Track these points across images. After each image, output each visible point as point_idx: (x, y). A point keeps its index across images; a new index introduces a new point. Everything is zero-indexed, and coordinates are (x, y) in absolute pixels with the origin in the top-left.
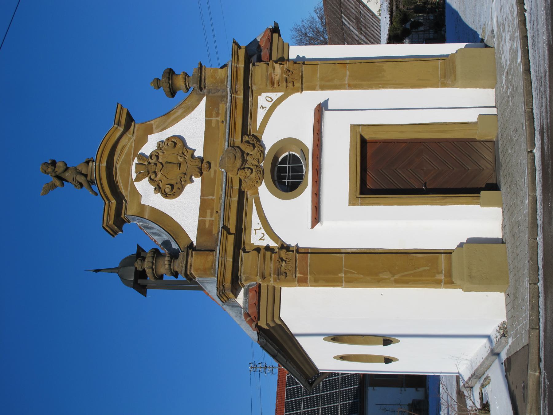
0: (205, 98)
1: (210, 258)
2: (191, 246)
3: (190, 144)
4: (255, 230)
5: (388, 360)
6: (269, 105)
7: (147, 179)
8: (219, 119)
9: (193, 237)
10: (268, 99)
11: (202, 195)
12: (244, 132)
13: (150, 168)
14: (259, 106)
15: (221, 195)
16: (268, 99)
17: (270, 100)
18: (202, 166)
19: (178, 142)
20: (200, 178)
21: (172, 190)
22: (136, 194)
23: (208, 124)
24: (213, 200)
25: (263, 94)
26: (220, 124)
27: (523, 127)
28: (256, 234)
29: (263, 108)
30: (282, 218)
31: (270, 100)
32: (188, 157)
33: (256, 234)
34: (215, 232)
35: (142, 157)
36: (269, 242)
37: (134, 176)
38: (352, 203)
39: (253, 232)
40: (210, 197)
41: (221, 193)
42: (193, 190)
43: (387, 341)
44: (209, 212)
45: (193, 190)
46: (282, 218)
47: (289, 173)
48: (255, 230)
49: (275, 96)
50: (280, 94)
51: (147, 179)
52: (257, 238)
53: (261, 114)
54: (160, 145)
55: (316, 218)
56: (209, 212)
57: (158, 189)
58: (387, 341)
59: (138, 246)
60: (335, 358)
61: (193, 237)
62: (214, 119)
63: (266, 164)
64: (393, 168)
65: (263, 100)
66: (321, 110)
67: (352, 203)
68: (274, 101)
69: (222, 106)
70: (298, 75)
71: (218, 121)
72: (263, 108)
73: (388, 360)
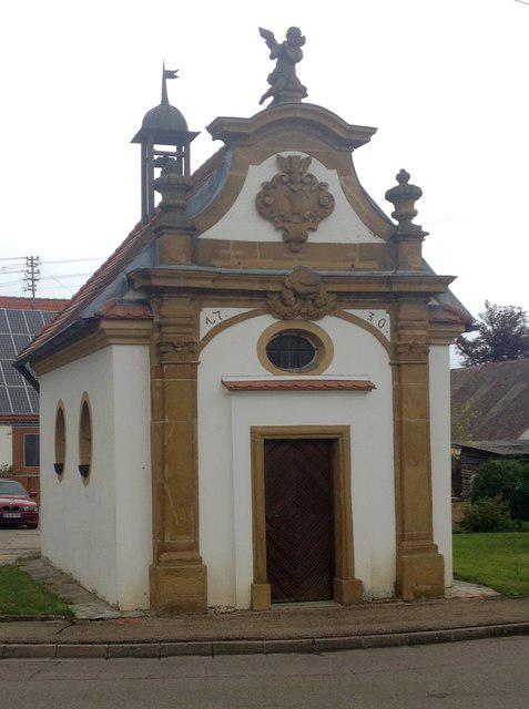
0: (383, 241)
1: (183, 259)
2: (193, 230)
5: (59, 468)
6: (374, 323)
8: (358, 264)
9: (210, 234)
11: (261, 244)
12: (340, 295)
13: (292, 175)
14: (373, 311)
19: (324, 207)
20: (281, 240)
21: (264, 207)
22: (259, 160)
23: (352, 247)
26: (351, 263)
30: (233, 347)
32: (310, 224)
34: (216, 262)
35: (308, 161)
36: (204, 329)
37: (285, 154)
39: (217, 309)
42: (266, 233)
43: (85, 470)
45: (266, 233)
46: (233, 347)
47: (293, 351)
49: (386, 331)
50: (388, 337)
52: (209, 316)
53: (363, 314)
54: (323, 186)
55: (235, 388)
57: (267, 188)
58: (85, 470)
59: (373, 131)
60: (60, 402)
61: (210, 234)
62: (356, 254)
63: (298, 324)
64: (301, 477)
65: (381, 317)
66: (367, 388)
67: (347, 428)
68: (381, 330)
69: (374, 264)
70: (407, 358)
71: (354, 260)
73: (59, 468)
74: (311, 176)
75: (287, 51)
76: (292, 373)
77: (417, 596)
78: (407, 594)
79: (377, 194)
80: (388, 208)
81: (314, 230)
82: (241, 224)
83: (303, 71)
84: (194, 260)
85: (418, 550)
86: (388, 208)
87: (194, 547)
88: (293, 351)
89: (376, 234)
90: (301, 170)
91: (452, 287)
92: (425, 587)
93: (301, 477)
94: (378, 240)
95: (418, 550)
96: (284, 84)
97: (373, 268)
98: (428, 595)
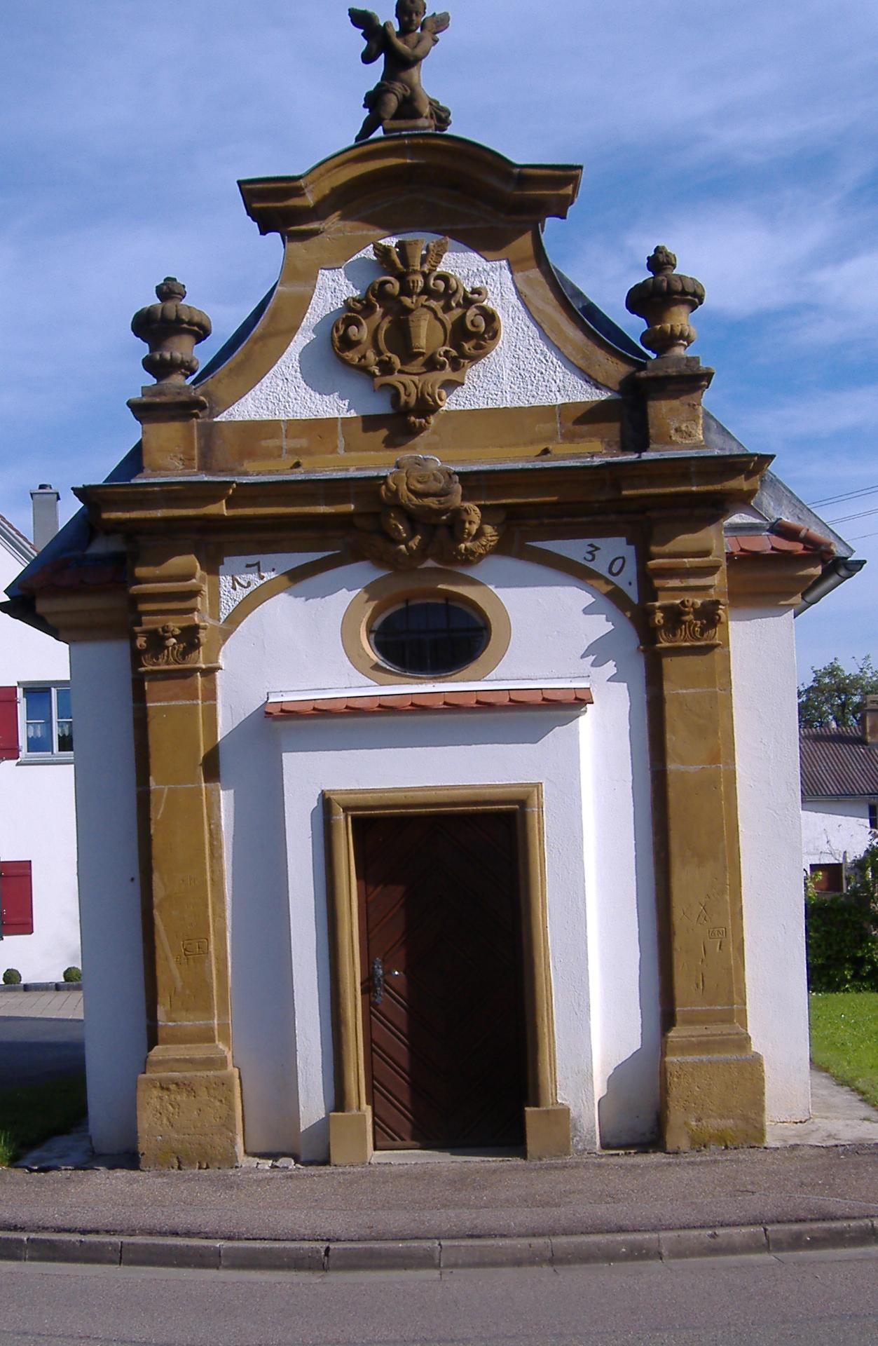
3: (473, 373)
4: (258, 564)
7: (449, 131)
10: (618, 563)
14: (597, 542)
15: (347, 470)
16: (618, 563)
17: (615, 570)
18: (401, 421)
19: (472, 335)
21: (339, 350)
24: (334, 451)
25: (632, 548)
27: (738, 1161)
28: (248, 566)
29: (590, 553)
31: (615, 570)
32: (447, 374)
33: (248, 566)
34: (248, 465)
38: (538, 786)
40: (341, 443)
41: (352, 469)
44: (303, 443)
48: (258, 564)
51: (449, 131)
52: (231, 587)
53: (573, 549)
56: (303, 443)
65: (612, 551)
67: (538, 786)
72: (590, 553)
74: (444, 278)
75: (393, 47)
76: (421, 681)
77: (699, 1144)
78: (676, 1137)
79: (610, 299)
80: (633, 326)
81: (450, 385)
82: (284, 393)
83: (433, 80)
84: (205, 467)
85: (704, 1046)
86: (633, 326)
87: (743, 1042)
88: (430, 636)
89: (597, 385)
90: (426, 268)
91: (771, 467)
92: (714, 1124)
93: (449, 890)
94: (603, 396)
95: (700, 1044)
96: (393, 104)
97: (594, 452)
98: (724, 1142)
